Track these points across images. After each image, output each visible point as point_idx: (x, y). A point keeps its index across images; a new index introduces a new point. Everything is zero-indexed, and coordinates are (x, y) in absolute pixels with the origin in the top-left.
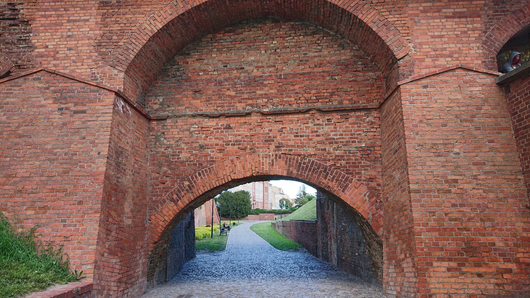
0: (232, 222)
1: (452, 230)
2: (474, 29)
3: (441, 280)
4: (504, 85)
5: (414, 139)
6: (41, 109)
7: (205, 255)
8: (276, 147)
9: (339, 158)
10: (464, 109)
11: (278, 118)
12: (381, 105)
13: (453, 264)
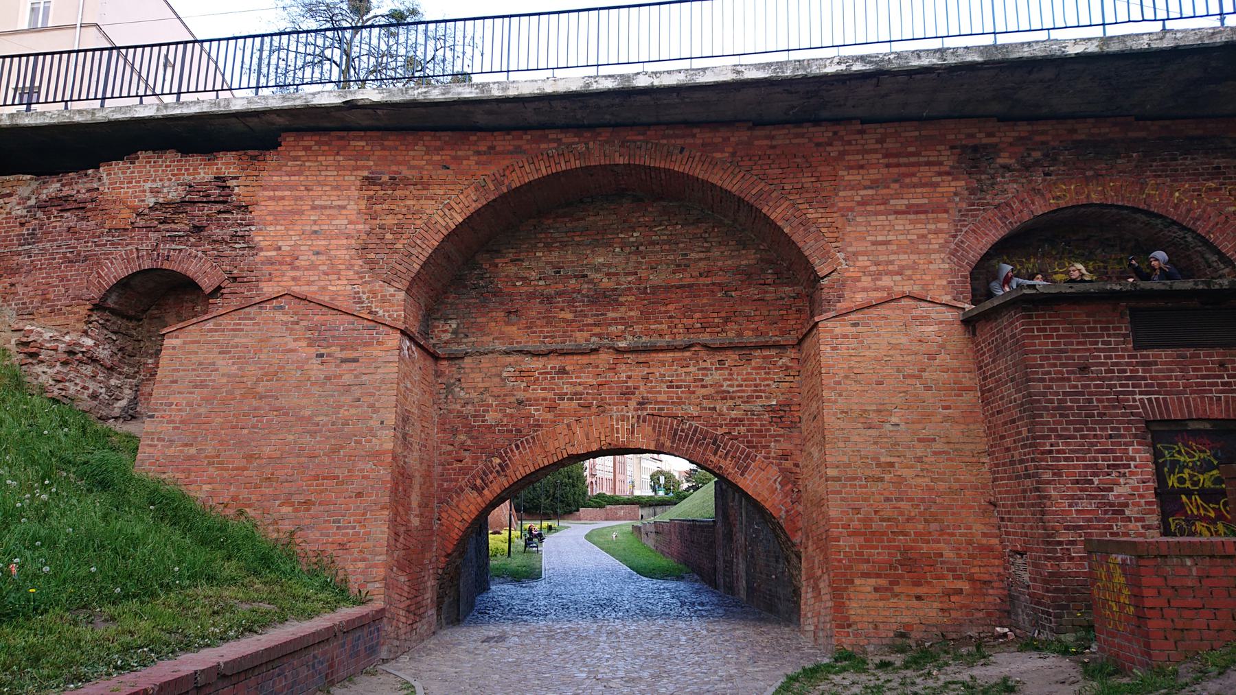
0: (545, 524)
1: (884, 534)
2: (937, 232)
3: (864, 603)
4: (970, 323)
5: (836, 401)
6: (289, 355)
7: (506, 586)
8: (639, 403)
9: (737, 422)
10: (909, 358)
11: (642, 358)
12: (801, 342)
13: (883, 582)
